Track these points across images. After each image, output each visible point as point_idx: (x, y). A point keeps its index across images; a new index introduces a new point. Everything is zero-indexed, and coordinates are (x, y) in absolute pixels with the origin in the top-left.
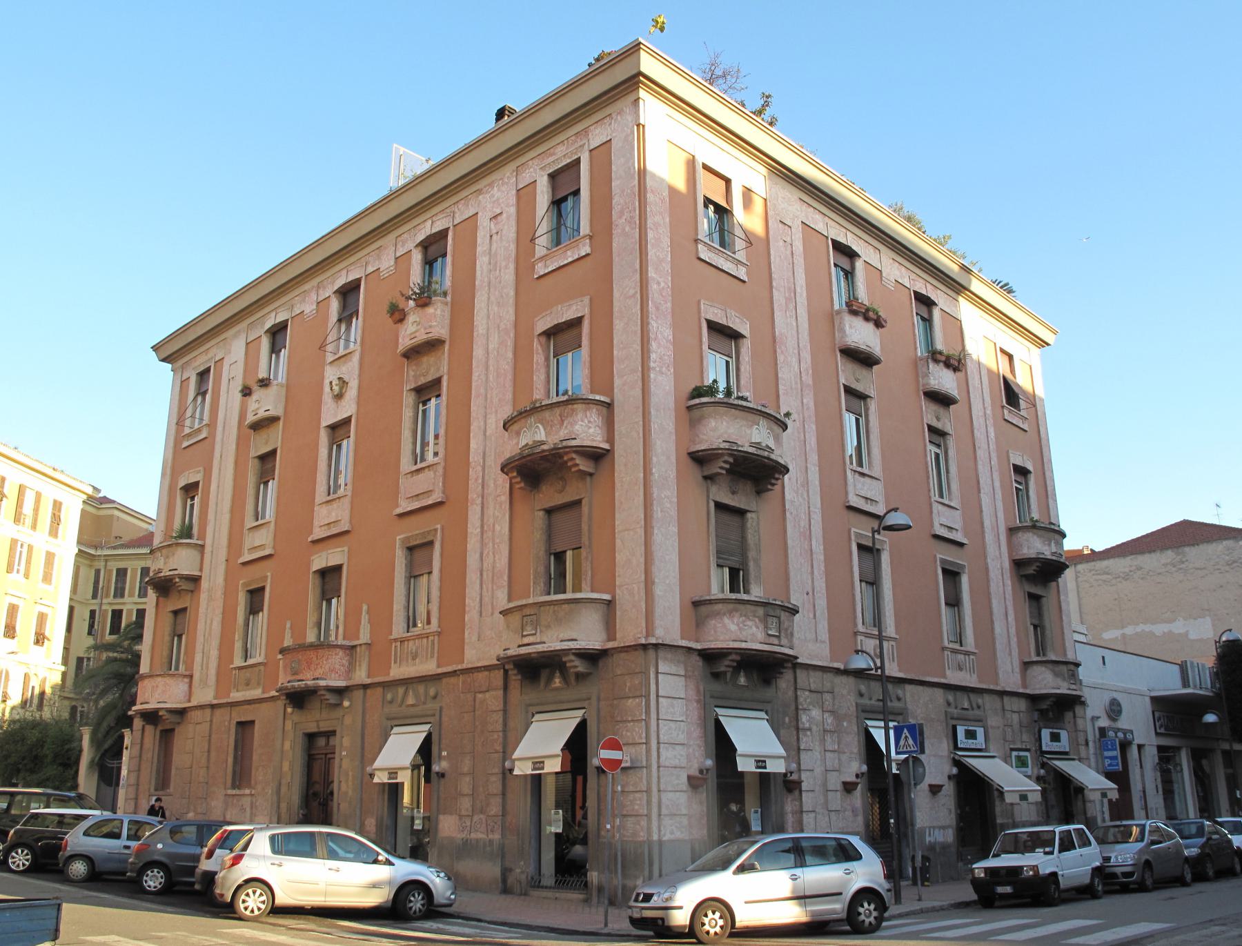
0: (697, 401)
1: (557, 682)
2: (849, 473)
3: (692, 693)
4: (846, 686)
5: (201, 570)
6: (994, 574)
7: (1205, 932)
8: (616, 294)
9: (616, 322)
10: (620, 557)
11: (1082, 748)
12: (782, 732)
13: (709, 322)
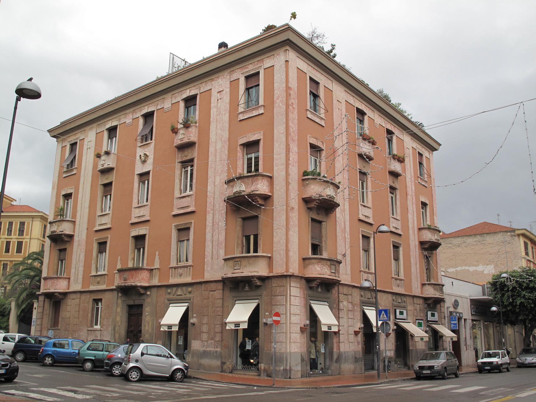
0: (306, 177)
1: (247, 288)
2: (360, 205)
3: (302, 294)
4: (356, 293)
5: (74, 232)
6: (412, 247)
7: (499, 389)
8: (275, 131)
9: (275, 143)
10: (275, 240)
11: (443, 319)
12: (334, 310)
13: (310, 144)
